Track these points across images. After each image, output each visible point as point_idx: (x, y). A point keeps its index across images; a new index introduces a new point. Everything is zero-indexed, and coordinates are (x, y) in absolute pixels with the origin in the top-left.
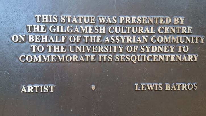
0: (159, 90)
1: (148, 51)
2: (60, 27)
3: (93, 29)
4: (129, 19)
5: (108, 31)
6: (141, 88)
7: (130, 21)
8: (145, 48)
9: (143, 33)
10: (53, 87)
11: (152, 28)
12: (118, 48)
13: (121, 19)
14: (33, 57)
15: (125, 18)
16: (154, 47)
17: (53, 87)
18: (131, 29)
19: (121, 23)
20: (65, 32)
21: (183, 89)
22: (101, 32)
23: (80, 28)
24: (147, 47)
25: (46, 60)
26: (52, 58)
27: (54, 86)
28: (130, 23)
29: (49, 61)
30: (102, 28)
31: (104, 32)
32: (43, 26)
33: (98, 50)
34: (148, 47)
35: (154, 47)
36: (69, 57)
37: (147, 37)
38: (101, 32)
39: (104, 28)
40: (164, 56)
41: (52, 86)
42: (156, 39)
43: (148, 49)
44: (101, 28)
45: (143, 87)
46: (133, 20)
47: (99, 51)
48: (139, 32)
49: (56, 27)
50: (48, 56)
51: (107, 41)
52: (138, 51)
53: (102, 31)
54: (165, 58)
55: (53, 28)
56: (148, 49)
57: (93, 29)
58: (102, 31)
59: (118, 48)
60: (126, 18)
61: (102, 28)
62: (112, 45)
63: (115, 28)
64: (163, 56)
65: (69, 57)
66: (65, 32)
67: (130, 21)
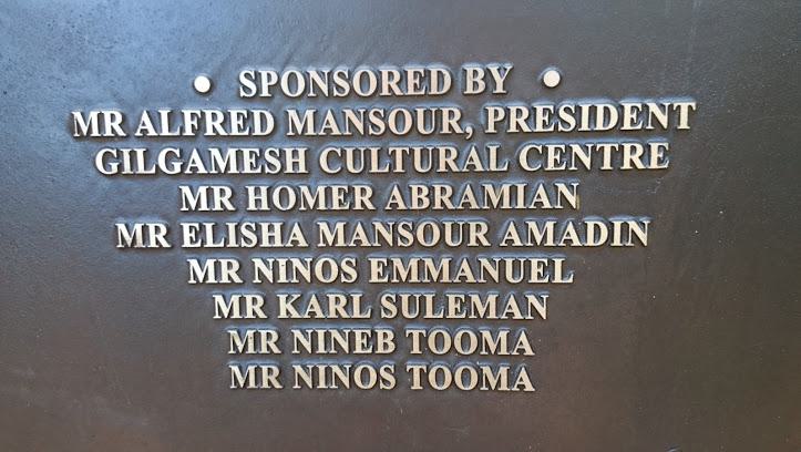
2: (133, 155)
3: (259, 158)
4: (526, 113)
5: (320, 166)
6: (446, 312)
7: (398, 84)
9: (346, 316)
10: (690, 107)
13: (491, 114)
14: (297, 191)
15: (507, 111)
16: (596, 225)
17: (690, 107)
18: (408, 157)
19: (491, 129)
20: (153, 171)
22: (289, 169)
23: (207, 154)
26: (336, 197)
27: (693, 105)
28: (398, 92)
30: (295, 153)
31: (302, 169)
32: (251, 153)
33: (352, 204)
35: (596, 225)
37: (545, 297)
38: (289, 169)
39: (301, 152)
40: (594, 148)
41: (684, 106)
44: (289, 152)
45: (452, 306)
46: (540, 118)
47: (358, 206)
49: (120, 154)
50: (321, 190)
51: (474, 166)
54: (597, 155)
55: (106, 157)
57: (259, 158)
58: (295, 164)
60: (513, 110)
61: (295, 153)
62: (595, 141)
63: (344, 152)
66: (153, 171)
67: (398, 84)
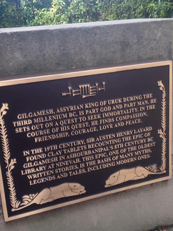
0: (82, 115)
1: (68, 110)
8: (66, 109)
11: (107, 148)
12: (134, 110)
21: (71, 110)
22: (50, 113)
24: (67, 108)
25: (39, 115)
29: (41, 115)
34: (68, 108)
36: (115, 113)
38: (50, 113)
42: (31, 135)
43: (68, 109)
48: (131, 100)
52: (112, 111)
53: (51, 113)
56: (68, 109)
59: (134, 110)
64: (69, 143)
65: (115, 113)
